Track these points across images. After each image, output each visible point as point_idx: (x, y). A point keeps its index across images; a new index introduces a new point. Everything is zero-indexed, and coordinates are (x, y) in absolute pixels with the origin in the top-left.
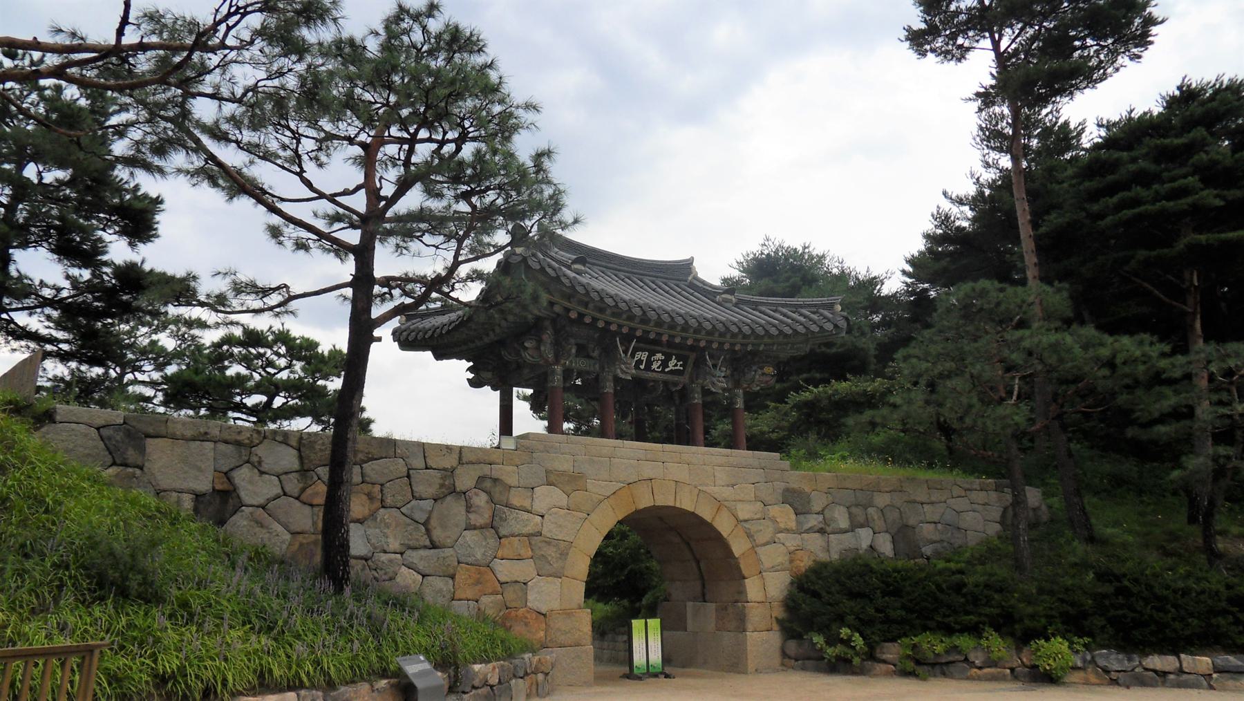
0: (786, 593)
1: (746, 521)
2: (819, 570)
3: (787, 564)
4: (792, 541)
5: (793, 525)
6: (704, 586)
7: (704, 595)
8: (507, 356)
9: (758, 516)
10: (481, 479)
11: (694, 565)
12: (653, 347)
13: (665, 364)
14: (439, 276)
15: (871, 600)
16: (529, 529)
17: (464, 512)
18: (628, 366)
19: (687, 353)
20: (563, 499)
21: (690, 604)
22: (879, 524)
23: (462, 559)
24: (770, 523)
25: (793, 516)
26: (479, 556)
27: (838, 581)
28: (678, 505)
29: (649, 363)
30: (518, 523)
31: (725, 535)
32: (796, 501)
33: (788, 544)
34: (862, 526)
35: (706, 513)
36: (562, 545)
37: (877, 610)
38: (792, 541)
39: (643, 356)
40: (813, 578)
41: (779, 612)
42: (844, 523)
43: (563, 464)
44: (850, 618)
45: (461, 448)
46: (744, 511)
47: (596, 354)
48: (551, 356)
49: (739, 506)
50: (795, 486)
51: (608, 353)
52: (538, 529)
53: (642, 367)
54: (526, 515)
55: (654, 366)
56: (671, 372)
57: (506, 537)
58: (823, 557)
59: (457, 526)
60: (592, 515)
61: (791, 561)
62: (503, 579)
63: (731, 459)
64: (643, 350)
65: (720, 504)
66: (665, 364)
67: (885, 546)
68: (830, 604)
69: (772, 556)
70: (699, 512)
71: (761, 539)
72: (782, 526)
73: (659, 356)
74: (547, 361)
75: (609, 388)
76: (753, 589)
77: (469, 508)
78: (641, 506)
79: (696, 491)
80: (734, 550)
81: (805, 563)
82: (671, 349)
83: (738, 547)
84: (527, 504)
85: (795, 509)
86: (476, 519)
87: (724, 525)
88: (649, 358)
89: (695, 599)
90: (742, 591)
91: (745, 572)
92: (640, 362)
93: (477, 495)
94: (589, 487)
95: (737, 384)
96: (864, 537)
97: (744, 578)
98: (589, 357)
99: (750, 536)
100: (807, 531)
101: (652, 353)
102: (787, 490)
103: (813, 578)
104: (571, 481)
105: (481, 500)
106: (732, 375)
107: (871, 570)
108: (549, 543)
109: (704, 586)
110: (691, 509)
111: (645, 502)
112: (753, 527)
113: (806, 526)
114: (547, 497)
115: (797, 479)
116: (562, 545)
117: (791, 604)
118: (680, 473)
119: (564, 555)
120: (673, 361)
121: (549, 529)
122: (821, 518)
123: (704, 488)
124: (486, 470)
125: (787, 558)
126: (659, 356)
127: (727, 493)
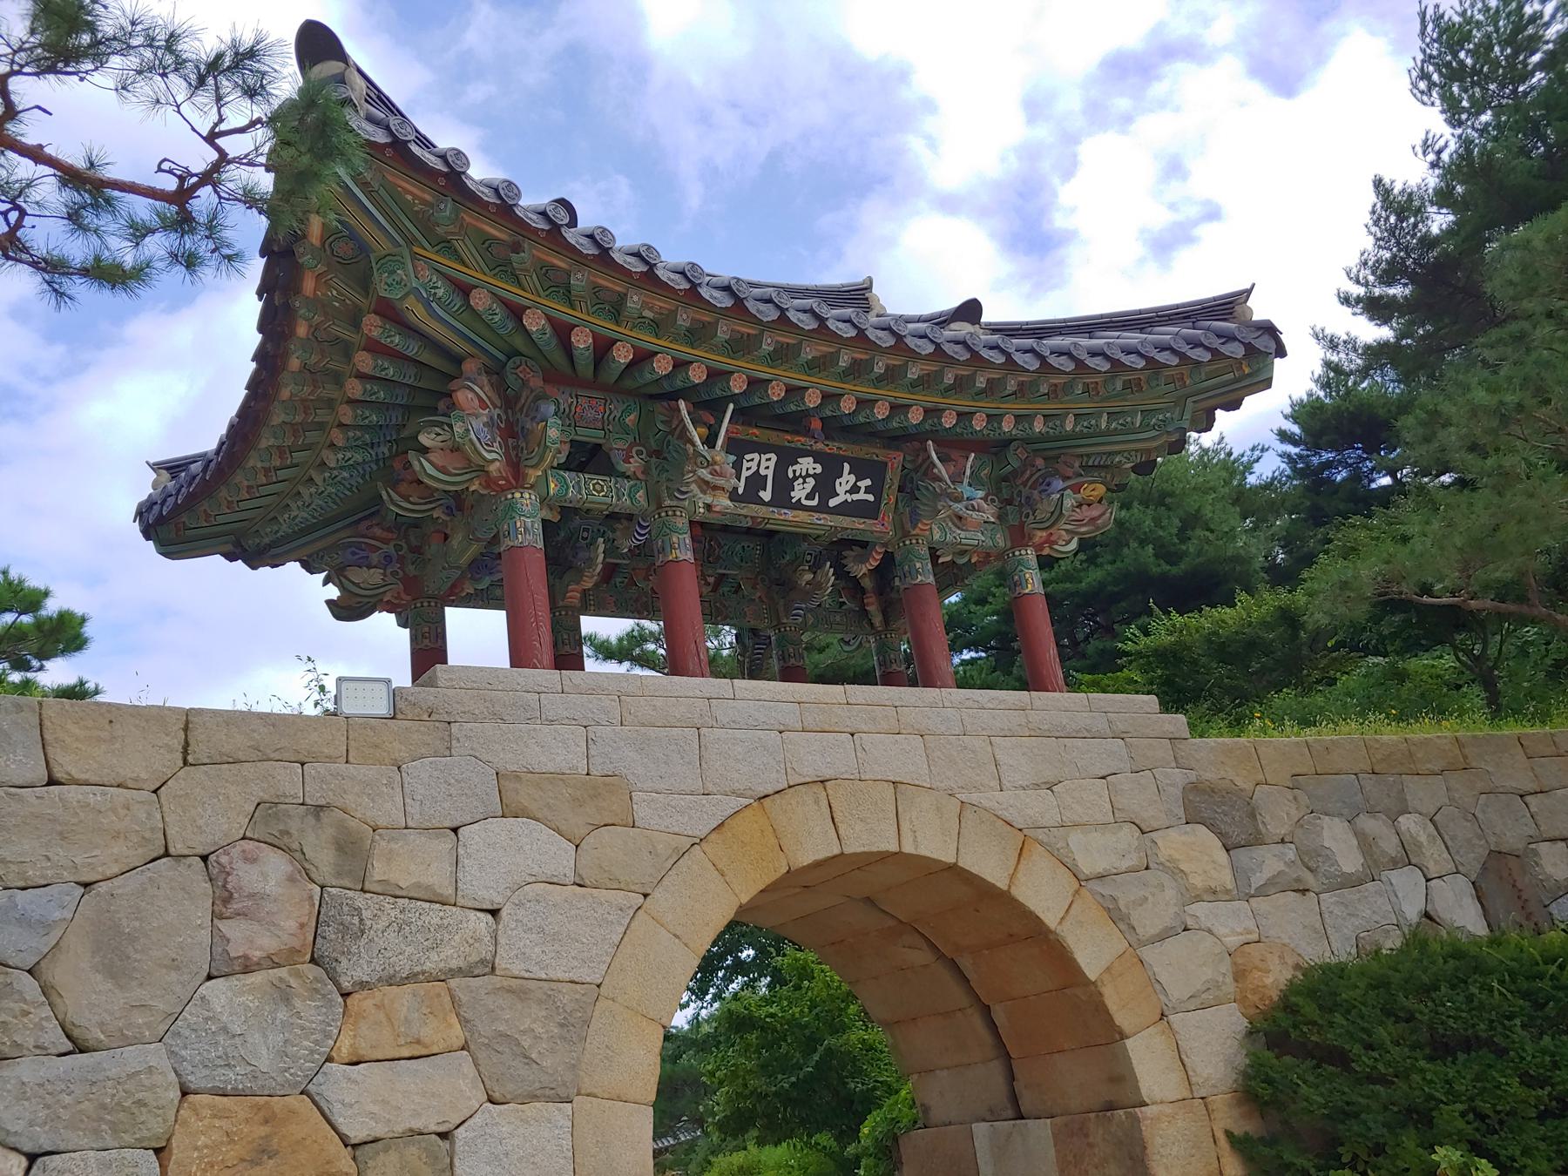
0: (1242, 1061)
1: (1101, 877)
2: (1320, 990)
3: (1230, 987)
4: (1230, 923)
5: (1226, 878)
6: (1011, 1077)
7: (1014, 1099)
8: (396, 504)
9: (1124, 865)
10: (266, 809)
11: (978, 1022)
12: (785, 439)
13: (824, 487)
14: (119, 266)
15: (1501, 1052)
16: (449, 956)
17: (202, 914)
18: (723, 479)
19: (875, 453)
20: (558, 856)
21: (981, 1129)
22: (1435, 857)
23: (194, 1081)
24: (1165, 879)
25: (1222, 856)
26: (264, 1060)
27: (1388, 1013)
28: (908, 848)
29: (783, 485)
30: (385, 942)
31: (1050, 920)
32: (1225, 815)
33: (1221, 930)
34: (1395, 864)
35: (990, 866)
36: (567, 996)
37: (1528, 1081)
38: (1230, 923)
39: (766, 464)
40: (1310, 1009)
41: (1228, 1118)
42: (1350, 862)
43: (557, 751)
44: (1450, 1116)
45: (189, 713)
46: (1093, 853)
47: (634, 465)
48: (494, 457)
49: (1076, 839)
50: (1209, 775)
51: (665, 455)
52: (484, 951)
53: (766, 495)
54: (434, 915)
55: (799, 492)
56: (845, 509)
57: (363, 985)
58: (1315, 953)
59: (174, 965)
60: (657, 894)
61: (1239, 975)
62: (356, 1133)
63: (1034, 716)
64: (762, 449)
65: (1024, 842)
66: (824, 487)
67: (1464, 916)
68: (1383, 1080)
69: (1184, 967)
70: (969, 863)
71: (1147, 923)
72: (1197, 881)
73: (807, 464)
74: (489, 482)
75: (683, 550)
76: (1150, 1065)
77: (224, 902)
78: (805, 859)
79: (954, 806)
80: (1047, 921)
81: (1276, 977)
82: (846, 437)
83: (1093, 951)
84: (437, 877)
85: (1220, 835)
86: (242, 937)
87: (1042, 893)
88: (780, 470)
89: (992, 1116)
90: (1122, 1077)
91: (1122, 1019)
92: (757, 481)
93: (250, 859)
94: (641, 813)
95: (1019, 537)
96: (1407, 895)
97: (1123, 1036)
98: (609, 470)
99: (1116, 915)
100: (1261, 892)
101: (787, 457)
102: (1193, 788)
103: (1310, 1009)
104: (596, 802)
105: (267, 874)
106: (1001, 517)
107: (1479, 968)
108: (521, 994)
109: (1011, 1077)
110: (948, 857)
111: (813, 844)
112: (1126, 894)
113: (1258, 880)
114: (505, 855)
115: (1220, 754)
116: (567, 996)
117: (1266, 1092)
118: (896, 757)
119: (574, 1027)
120: (846, 480)
121: (521, 951)
122: (1290, 852)
123: (974, 797)
124: (287, 780)
125: (1226, 966)
126: (807, 464)
127: (1034, 808)
